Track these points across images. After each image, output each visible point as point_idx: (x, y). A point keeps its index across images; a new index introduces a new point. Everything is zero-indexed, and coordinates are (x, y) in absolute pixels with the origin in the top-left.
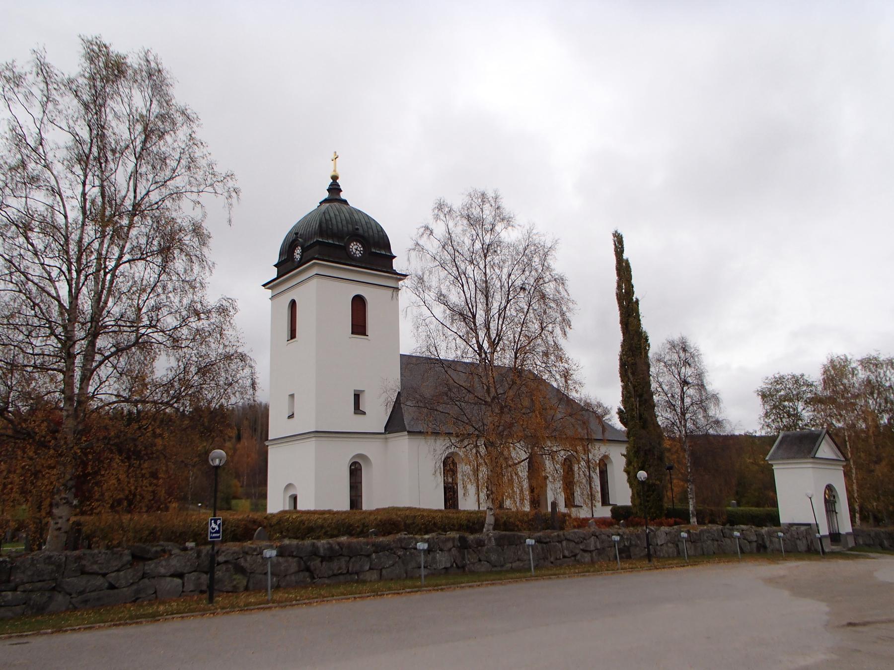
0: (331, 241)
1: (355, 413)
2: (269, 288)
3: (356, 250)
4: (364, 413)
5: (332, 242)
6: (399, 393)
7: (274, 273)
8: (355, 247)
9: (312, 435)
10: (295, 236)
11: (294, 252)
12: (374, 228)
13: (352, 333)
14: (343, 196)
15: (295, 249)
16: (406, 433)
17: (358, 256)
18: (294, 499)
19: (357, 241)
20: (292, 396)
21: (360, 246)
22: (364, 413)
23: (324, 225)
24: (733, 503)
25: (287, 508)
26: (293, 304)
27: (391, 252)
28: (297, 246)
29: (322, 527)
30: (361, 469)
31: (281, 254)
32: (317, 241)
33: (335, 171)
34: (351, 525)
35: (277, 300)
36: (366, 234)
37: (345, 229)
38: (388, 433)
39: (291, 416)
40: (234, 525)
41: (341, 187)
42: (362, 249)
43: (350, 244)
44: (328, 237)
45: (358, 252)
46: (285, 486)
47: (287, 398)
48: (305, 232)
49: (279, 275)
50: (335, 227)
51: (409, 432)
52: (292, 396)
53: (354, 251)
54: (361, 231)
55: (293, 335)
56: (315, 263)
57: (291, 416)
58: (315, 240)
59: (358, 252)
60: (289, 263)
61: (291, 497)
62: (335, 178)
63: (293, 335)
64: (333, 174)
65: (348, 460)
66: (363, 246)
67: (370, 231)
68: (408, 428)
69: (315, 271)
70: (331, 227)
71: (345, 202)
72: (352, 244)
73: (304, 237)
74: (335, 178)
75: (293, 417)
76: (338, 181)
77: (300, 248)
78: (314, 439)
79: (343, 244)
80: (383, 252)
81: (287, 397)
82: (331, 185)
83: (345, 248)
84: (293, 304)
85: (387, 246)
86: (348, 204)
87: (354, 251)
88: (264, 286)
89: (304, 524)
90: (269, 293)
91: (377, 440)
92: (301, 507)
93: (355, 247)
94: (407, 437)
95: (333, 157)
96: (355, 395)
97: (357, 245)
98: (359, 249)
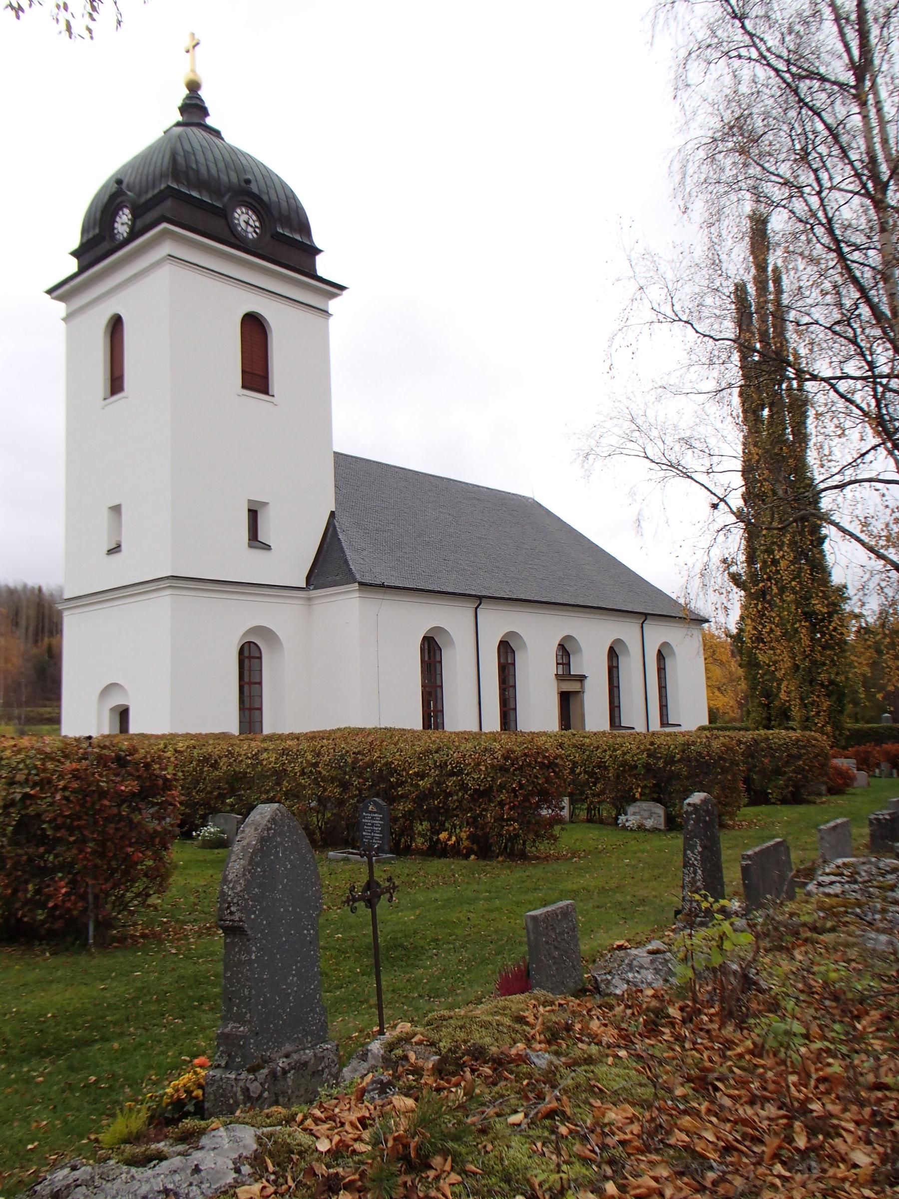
0: (195, 194)
1: (250, 546)
2: (60, 298)
3: (247, 223)
4: (268, 547)
5: (198, 196)
6: (332, 514)
7: (72, 265)
8: (245, 217)
9: (162, 584)
10: (116, 185)
11: (114, 221)
12: (279, 190)
13: (244, 387)
14: (209, 121)
15: (117, 214)
16: (356, 586)
17: (250, 236)
18: (123, 714)
19: (249, 206)
20: (116, 510)
21: (254, 218)
22: (268, 547)
23: (181, 160)
24: (887, 717)
25: (107, 732)
26: (116, 325)
27: (312, 241)
28: (121, 209)
29: (280, 774)
30: (260, 658)
31: (84, 231)
32: (169, 187)
33: (193, 71)
34: (393, 771)
35: (77, 321)
36: (265, 198)
37: (224, 177)
38: (315, 589)
39: (115, 549)
40: (20, 777)
41: (208, 104)
42: (257, 224)
43: (234, 211)
44: (190, 186)
45: (250, 229)
46: (103, 687)
47: (104, 516)
48: (139, 177)
49: (82, 270)
50: (203, 170)
51: (361, 584)
52: (116, 510)
53: (243, 225)
54: (254, 187)
55: (116, 384)
56: (166, 232)
57: (115, 549)
58: (163, 187)
59: (250, 229)
60: (105, 246)
61: (113, 710)
62: (194, 87)
63: (116, 384)
64: (191, 76)
65: (237, 642)
66: (260, 219)
67: (272, 192)
68: (358, 577)
69: (167, 248)
70: (194, 166)
71: (217, 133)
72: (239, 211)
73: (137, 188)
74: (194, 87)
75: (120, 551)
76: (199, 93)
77: (127, 211)
78: (168, 592)
79: (220, 206)
80: (298, 237)
81: (105, 512)
82: (188, 97)
83: (225, 215)
84: (116, 325)
85: (304, 227)
86: (222, 139)
87: (243, 225)
88: (50, 292)
89: (215, 766)
90: (60, 308)
91: (294, 602)
92: (135, 728)
93: (245, 217)
94: (357, 594)
95: (188, 43)
96: (249, 510)
97: (247, 214)
98: (251, 222)
